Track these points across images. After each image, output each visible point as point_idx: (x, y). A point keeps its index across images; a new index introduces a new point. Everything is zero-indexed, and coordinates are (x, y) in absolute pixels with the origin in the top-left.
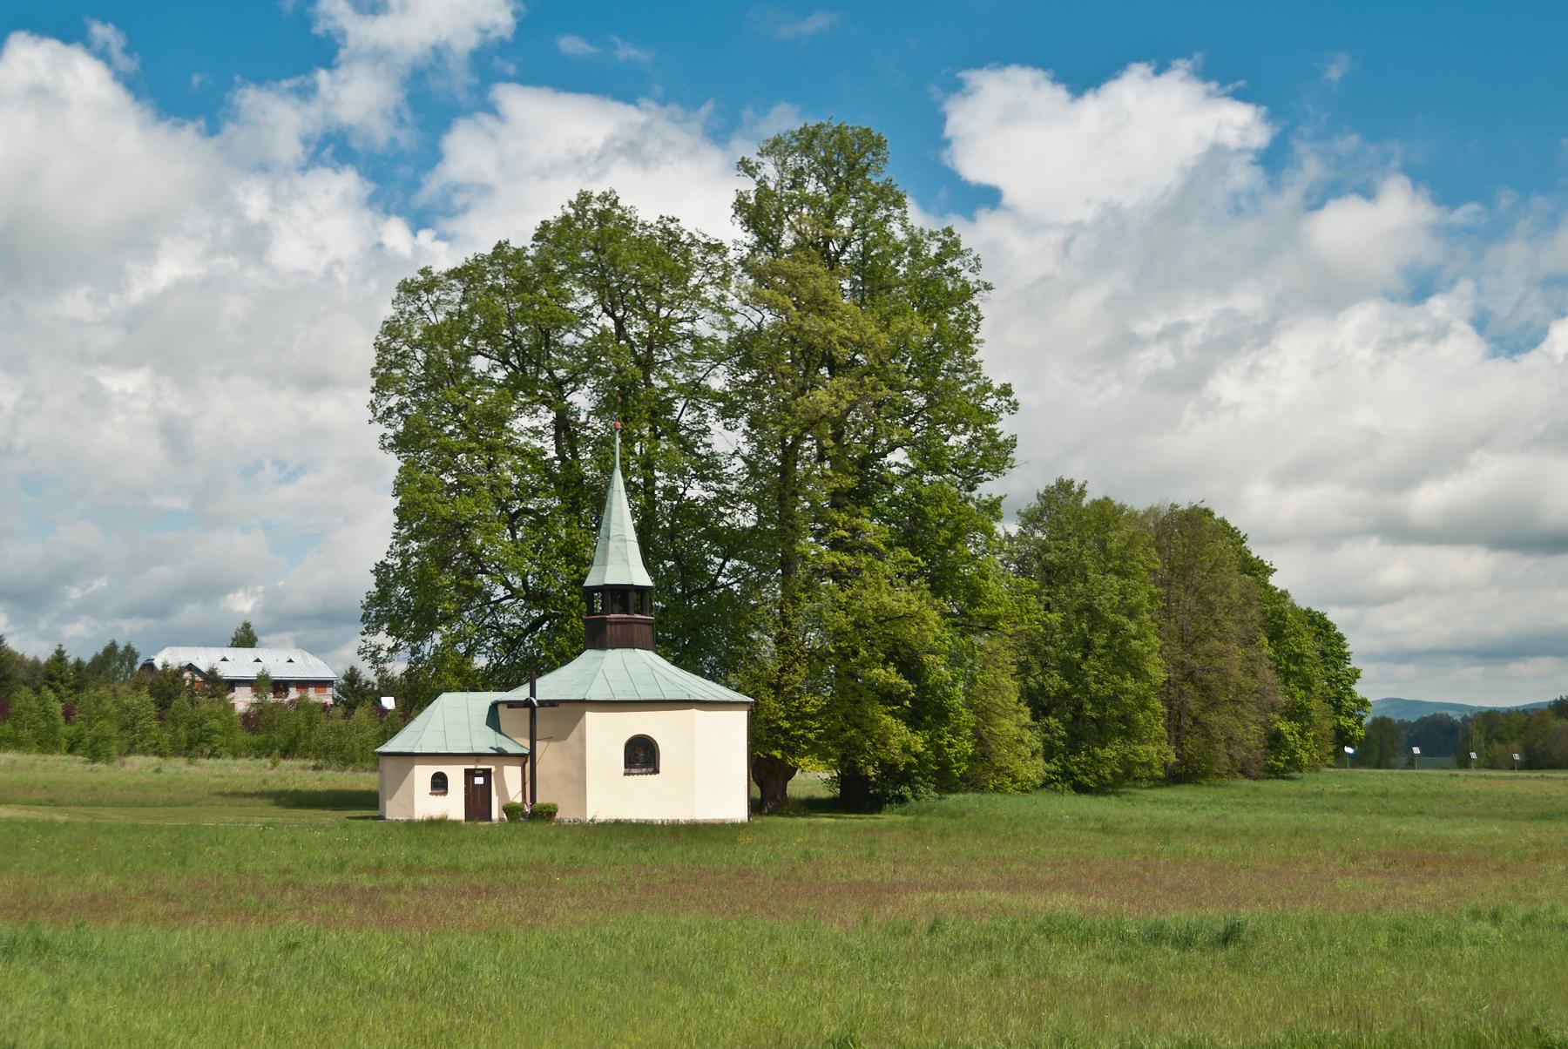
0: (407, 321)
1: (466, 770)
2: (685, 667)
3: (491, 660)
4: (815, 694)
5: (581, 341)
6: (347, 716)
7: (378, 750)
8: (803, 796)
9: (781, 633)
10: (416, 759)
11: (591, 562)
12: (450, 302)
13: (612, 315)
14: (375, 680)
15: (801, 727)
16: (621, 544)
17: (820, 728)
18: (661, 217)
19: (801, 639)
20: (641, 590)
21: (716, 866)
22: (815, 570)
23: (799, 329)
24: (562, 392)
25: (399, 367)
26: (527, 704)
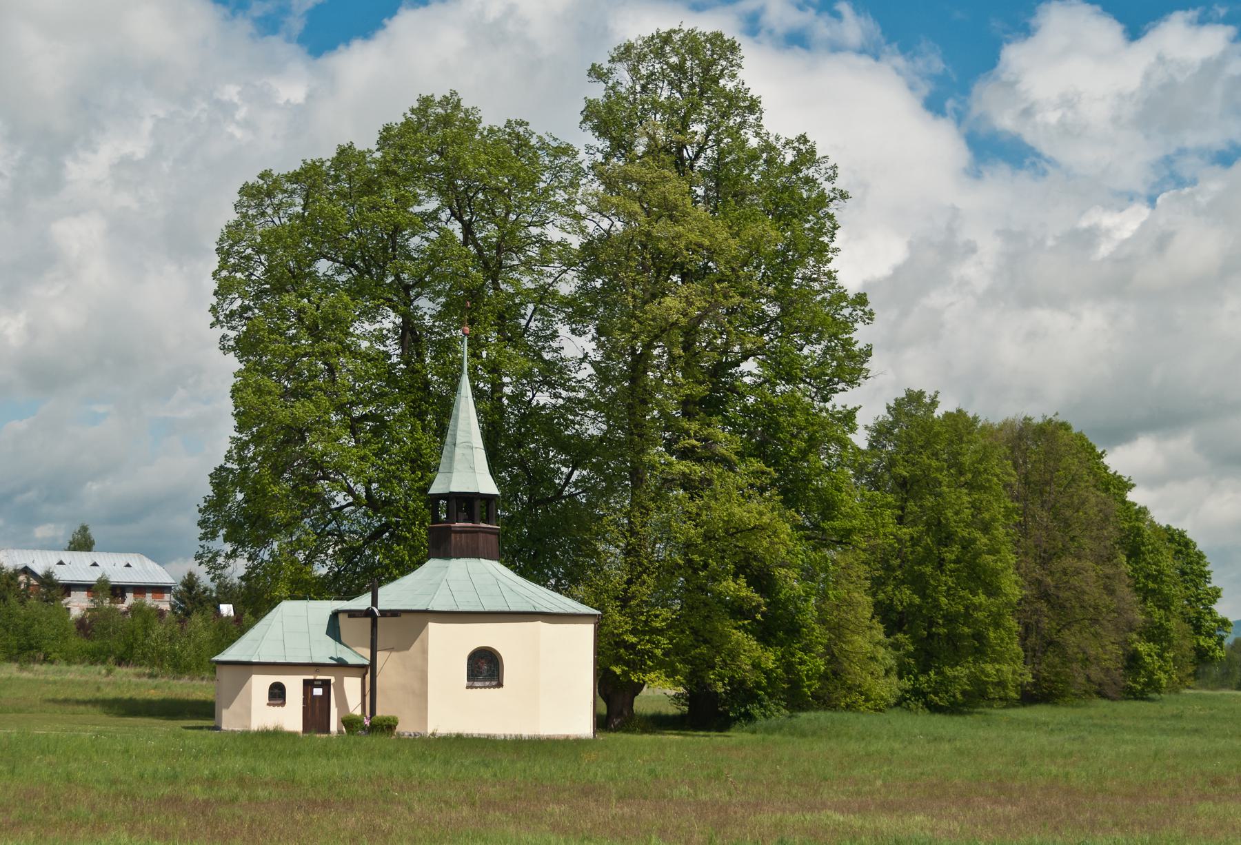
1: (304, 680)
10: (254, 668)
20: (488, 498)
26: (368, 613)
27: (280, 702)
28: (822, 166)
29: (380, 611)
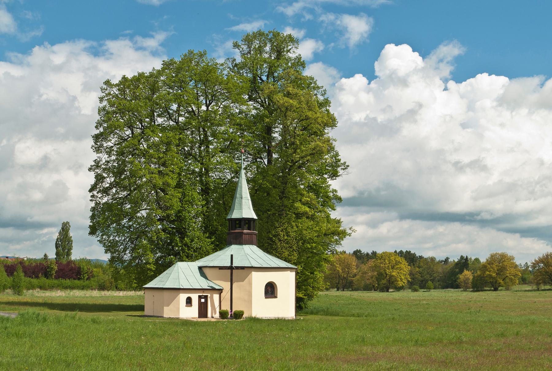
1: (199, 296)
10: (181, 291)
20: (253, 220)
27: (190, 305)
28: (320, 90)
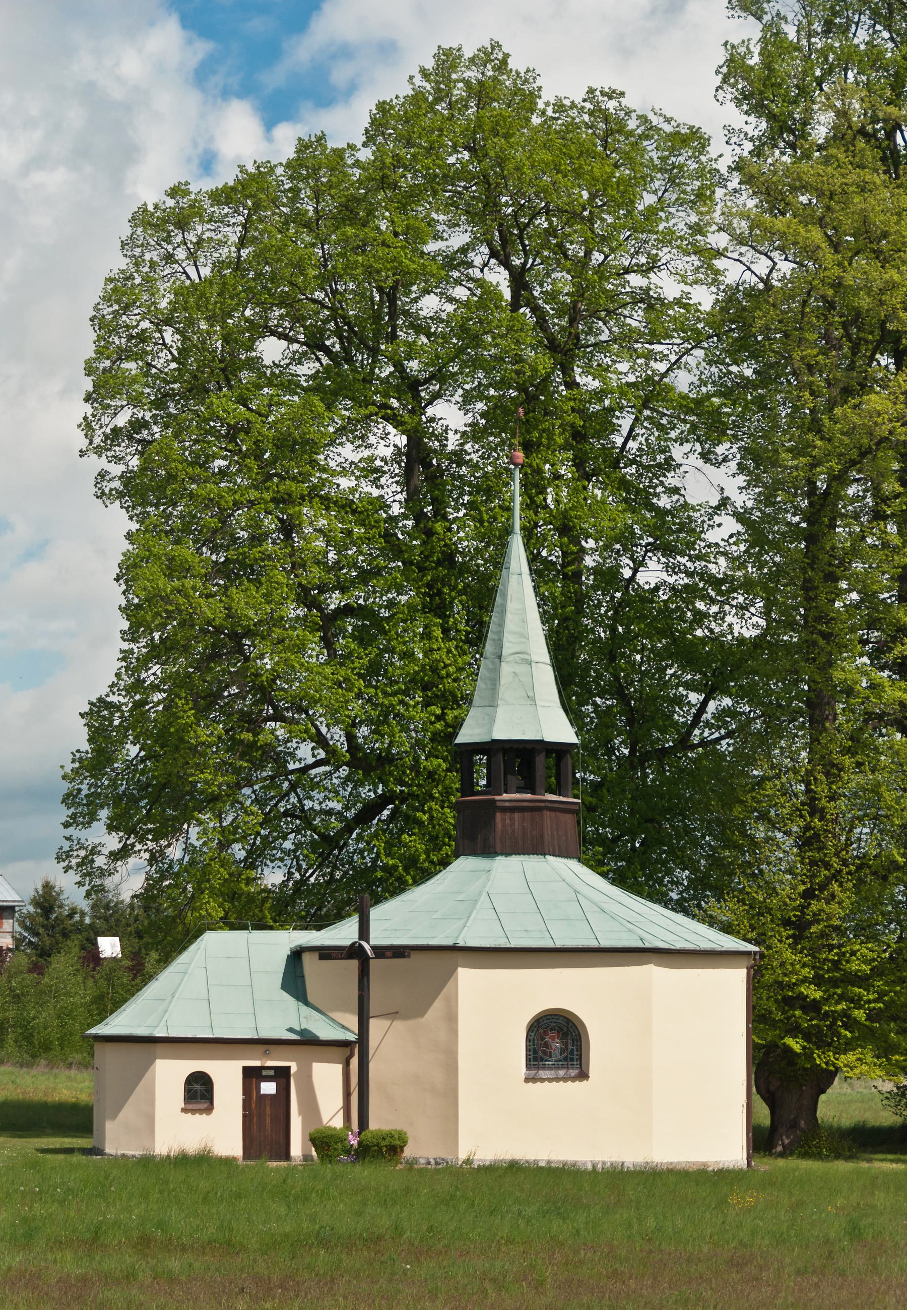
0: (146, 279)
1: (245, 1069)
2: (635, 889)
3: (290, 873)
4: (868, 939)
5: (450, 308)
6: (37, 969)
7: (93, 1031)
8: (846, 1122)
9: (807, 828)
10: (159, 1047)
11: (468, 700)
12: (221, 243)
13: (506, 264)
14: (84, 905)
15: (842, 998)
16: (523, 669)
17: (875, 1001)
18: (591, 91)
19: (843, 838)
20: (558, 750)
21: (690, 1248)
22: (869, 716)
23: (838, 285)
24: (416, 396)
25: (135, 357)
26: (354, 952)
27: (203, 1106)
29: (374, 948)
